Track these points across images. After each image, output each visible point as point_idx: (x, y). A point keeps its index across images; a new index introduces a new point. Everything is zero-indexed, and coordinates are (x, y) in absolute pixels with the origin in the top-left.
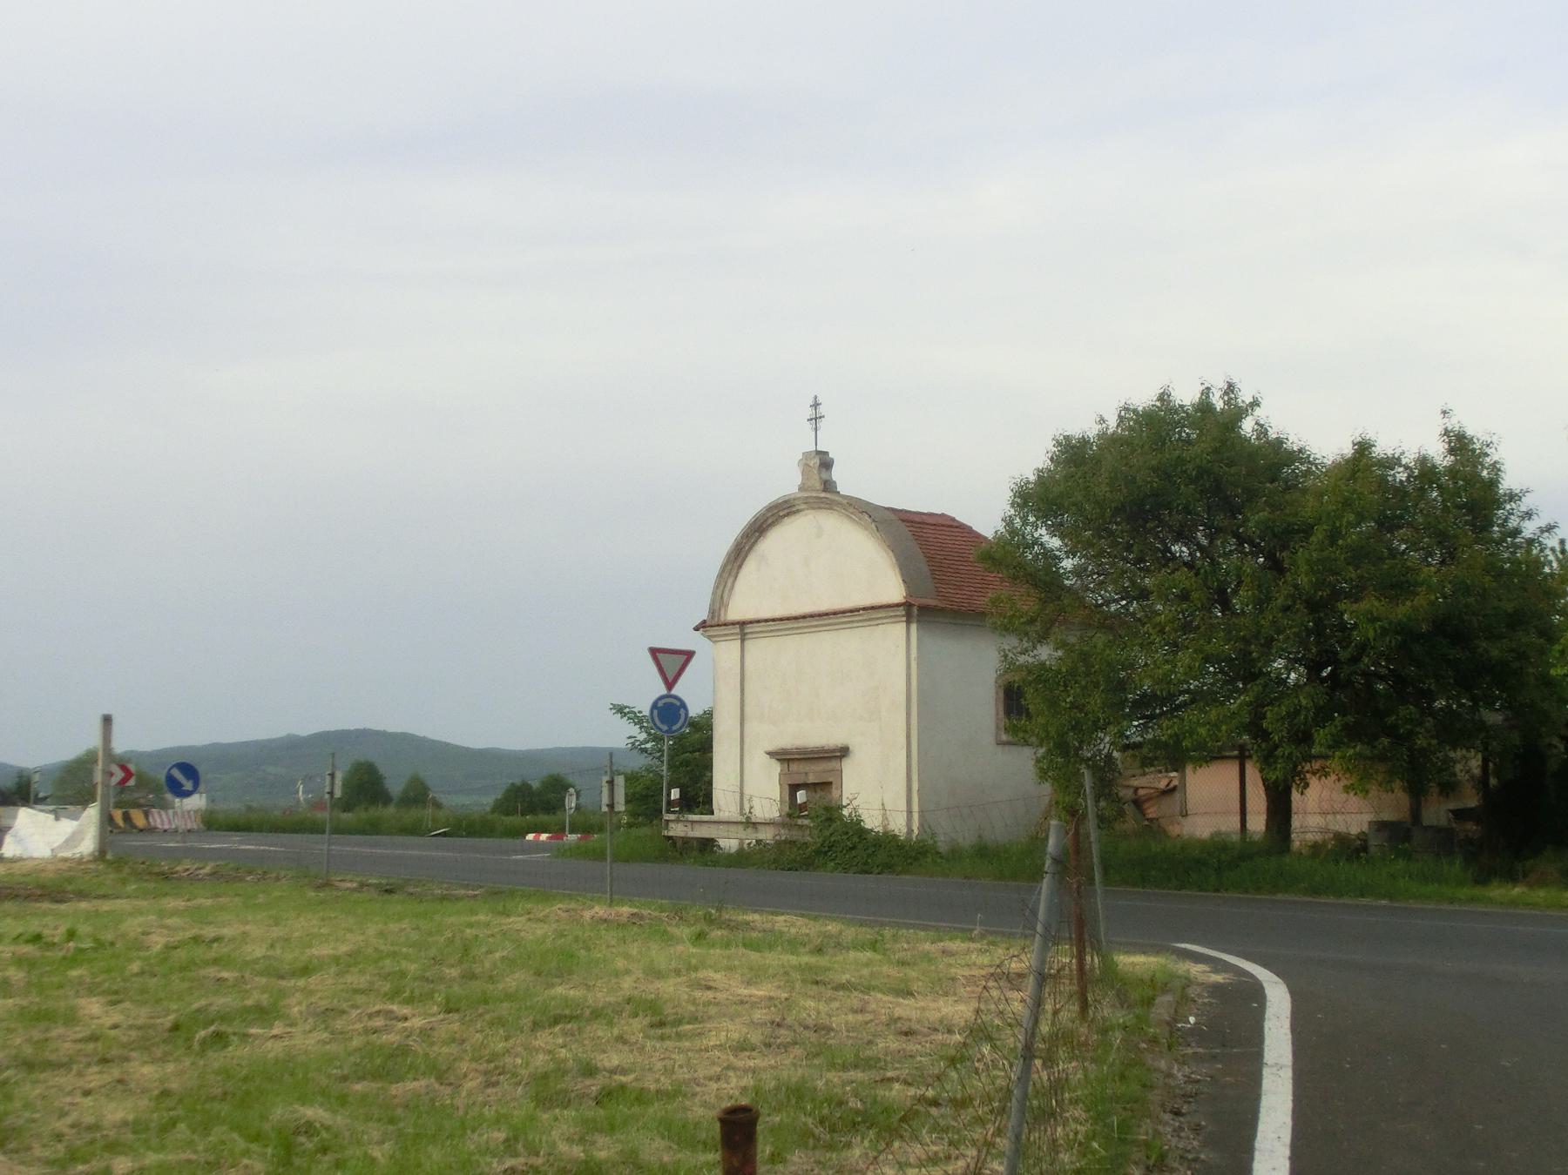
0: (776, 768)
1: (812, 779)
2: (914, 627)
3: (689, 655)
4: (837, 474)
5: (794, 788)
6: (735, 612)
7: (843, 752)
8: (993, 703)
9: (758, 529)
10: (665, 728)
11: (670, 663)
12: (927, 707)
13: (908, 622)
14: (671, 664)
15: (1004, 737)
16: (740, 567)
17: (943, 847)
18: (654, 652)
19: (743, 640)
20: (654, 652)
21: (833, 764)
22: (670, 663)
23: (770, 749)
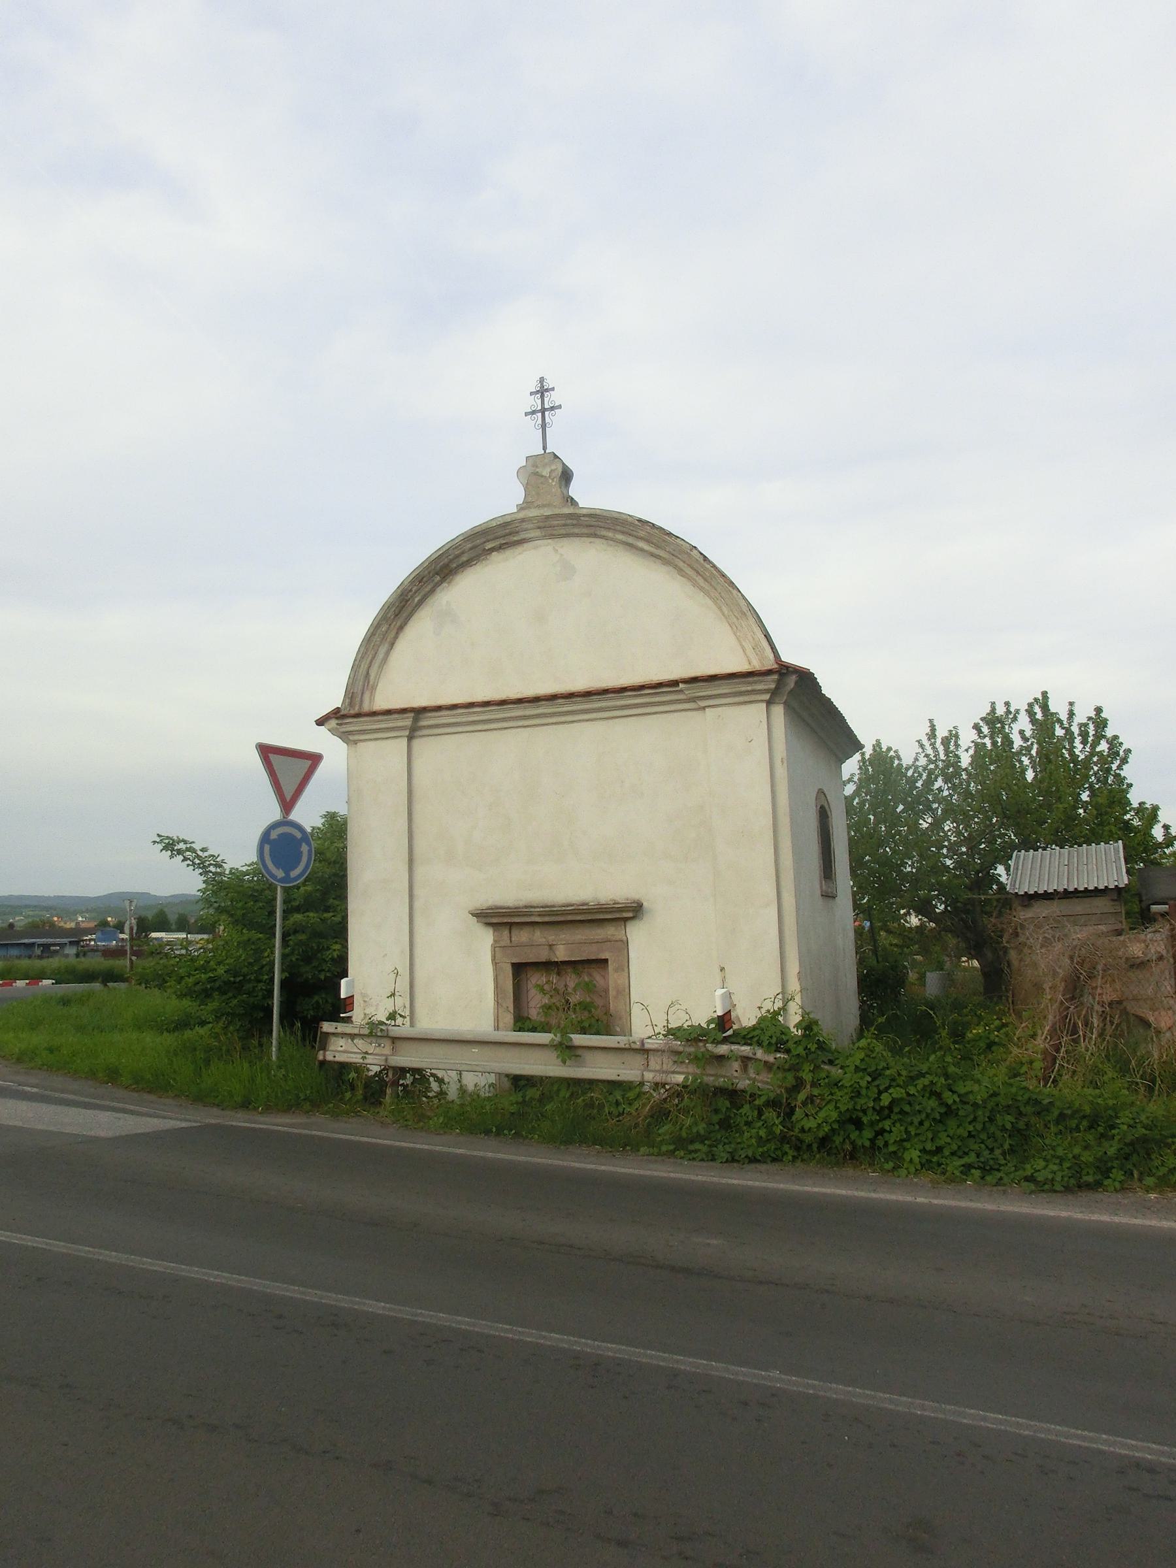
0: (486, 939)
1: (561, 954)
4: (574, 491)
5: (520, 969)
6: (383, 699)
7: (632, 912)
9: (442, 569)
10: (280, 874)
11: (287, 767)
14: (290, 772)
16: (401, 628)
18: (266, 751)
19: (410, 738)
20: (266, 751)
21: (610, 931)
22: (287, 767)
23: (515, 888)
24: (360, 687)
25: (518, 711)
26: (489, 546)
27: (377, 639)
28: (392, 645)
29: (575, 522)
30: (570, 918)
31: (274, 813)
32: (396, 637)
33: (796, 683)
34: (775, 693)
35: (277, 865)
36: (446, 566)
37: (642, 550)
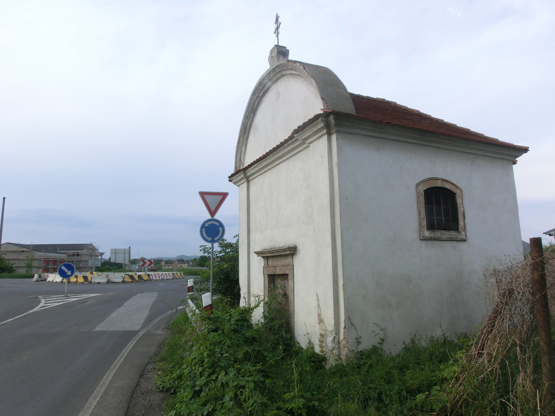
2: (334, 137)
3: (224, 195)
11: (213, 200)
12: (349, 209)
13: (329, 134)
15: (427, 234)
17: (536, 275)
18: (203, 194)
20: (203, 194)
21: (288, 261)
22: (213, 200)
25: (264, 163)
26: (261, 95)
27: (241, 144)
28: (246, 145)
30: (282, 253)
32: (247, 142)
33: (334, 119)
34: (327, 126)
35: (208, 236)
37: (295, 75)
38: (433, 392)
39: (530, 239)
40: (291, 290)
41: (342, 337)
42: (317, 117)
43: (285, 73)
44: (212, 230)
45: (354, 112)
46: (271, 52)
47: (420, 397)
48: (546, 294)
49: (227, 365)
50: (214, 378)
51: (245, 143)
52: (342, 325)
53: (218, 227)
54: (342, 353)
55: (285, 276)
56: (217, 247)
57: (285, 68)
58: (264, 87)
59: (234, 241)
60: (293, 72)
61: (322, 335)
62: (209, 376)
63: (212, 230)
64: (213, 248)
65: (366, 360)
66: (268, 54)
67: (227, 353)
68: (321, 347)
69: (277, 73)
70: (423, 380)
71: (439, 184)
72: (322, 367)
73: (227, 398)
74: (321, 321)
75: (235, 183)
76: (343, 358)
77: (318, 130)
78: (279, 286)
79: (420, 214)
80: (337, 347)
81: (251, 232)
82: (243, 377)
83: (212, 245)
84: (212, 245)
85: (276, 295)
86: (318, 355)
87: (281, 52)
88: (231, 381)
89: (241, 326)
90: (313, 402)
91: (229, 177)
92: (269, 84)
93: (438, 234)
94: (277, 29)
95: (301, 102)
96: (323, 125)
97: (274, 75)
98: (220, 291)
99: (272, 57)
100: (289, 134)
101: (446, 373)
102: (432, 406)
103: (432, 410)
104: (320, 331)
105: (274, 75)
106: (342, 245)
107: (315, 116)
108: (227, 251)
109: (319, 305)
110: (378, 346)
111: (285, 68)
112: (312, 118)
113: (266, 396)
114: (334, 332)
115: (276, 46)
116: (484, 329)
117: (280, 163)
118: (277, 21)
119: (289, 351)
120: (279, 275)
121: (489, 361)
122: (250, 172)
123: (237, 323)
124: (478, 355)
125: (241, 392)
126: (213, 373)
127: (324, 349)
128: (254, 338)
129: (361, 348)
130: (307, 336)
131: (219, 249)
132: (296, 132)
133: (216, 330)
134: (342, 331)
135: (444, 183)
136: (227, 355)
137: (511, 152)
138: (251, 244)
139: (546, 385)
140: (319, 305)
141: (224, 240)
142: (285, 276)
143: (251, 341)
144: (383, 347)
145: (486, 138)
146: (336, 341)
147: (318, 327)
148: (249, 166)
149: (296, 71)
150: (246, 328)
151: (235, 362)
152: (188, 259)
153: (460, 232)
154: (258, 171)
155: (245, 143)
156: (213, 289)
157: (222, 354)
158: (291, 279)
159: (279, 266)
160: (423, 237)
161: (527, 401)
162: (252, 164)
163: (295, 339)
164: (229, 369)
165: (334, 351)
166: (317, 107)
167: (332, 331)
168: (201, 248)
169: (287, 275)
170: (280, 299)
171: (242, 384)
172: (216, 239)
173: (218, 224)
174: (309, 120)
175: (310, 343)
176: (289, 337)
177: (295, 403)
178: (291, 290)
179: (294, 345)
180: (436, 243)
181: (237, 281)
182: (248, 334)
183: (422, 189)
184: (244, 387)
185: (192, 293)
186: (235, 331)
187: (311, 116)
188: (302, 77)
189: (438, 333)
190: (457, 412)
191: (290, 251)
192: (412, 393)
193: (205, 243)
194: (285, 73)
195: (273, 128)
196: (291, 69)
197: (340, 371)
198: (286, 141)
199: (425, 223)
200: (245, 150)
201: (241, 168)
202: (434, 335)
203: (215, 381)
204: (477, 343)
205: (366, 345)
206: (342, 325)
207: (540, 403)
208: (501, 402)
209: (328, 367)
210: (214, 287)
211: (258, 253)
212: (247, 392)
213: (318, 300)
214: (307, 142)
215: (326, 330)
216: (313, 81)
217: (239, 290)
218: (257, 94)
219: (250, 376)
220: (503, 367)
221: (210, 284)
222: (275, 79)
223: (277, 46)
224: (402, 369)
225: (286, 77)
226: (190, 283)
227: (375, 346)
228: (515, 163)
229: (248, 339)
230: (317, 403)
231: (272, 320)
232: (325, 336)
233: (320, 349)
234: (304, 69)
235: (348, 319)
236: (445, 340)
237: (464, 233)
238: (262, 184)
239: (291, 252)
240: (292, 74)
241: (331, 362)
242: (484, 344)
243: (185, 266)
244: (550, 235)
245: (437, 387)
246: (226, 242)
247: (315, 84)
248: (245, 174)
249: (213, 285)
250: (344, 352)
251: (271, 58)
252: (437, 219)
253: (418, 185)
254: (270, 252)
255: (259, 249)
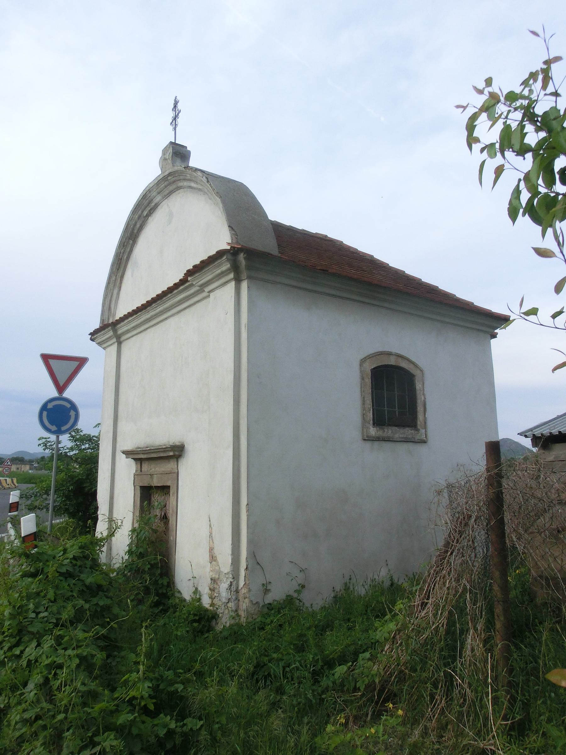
2: (244, 285)
3: (82, 362)
8: (357, 390)
11: (62, 368)
12: (260, 394)
13: (238, 280)
15: (373, 431)
16: (122, 277)
18: (46, 358)
20: (46, 358)
21: (170, 466)
22: (62, 368)
24: (107, 317)
26: (145, 213)
27: (111, 285)
29: (166, 183)
30: (162, 455)
31: (53, 393)
33: (245, 258)
34: (235, 268)
35: (51, 423)
36: (132, 232)
38: (360, 662)
39: (486, 443)
40: (173, 511)
41: (242, 583)
42: (220, 254)
43: (180, 184)
44: (59, 415)
45: (274, 250)
46: (165, 151)
47: (340, 670)
48: (502, 518)
49: (42, 631)
50: (18, 652)
51: (118, 283)
52: (243, 565)
53: (69, 410)
54: (241, 607)
55: (165, 489)
56: (66, 441)
57: (181, 177)
58: (150, 202)
59: (93, 433)
60: (193, 185)
61: (213, 580)
62: (10, 649)
63: (59, 415)
64: (59, 442)
65: (278, 617)
66: (159, 154)
67: (46, 610)
68: (212, 598)
69: (169, 184)
70: (349, 645)
71: (392, 361)
72: (210, 629)
73: (31, 686)
74: (213, 558)
75: (99, 344)
76: (242, 614)
77: (222, 273)
78: (156, 504)
79: (364, 402)
80: (234, 597)
81: (119, 420)
82: (65, 649)
83: (58, 437)
84: (58, 437)
85: (150, 518)
86: (207, 610)
87: (178, 153)
88: (44, 657)
89: (80, 566)
90: (176, 685)
91: (92, 334)
92: (158, 199)
93: (389, 432)
94: (175, 118)
95: (195, 230)
96: (229, 266)
97: (166, 187)
98: (67, 510)
99: (165, 159)
100: (181, 276)
101: (379, 635)
102: (356, 682)
103: (356, 689)
104: (211, 573)
105: (166, 187)
106: (248, 444)
107: (218, 252)
108: (83, 447)
109: (211, 534)
110: (295, 595)
111: (181, 177)
112: (214, 255)
113: (95, 678)
114: (231, 576)
115: (171, 143)
116: (431, 567)
117: (166, 319)
118: (175, 106)
119: (164, 604)
120: (157, 487)
121: (435, 615)
122: (122, 329)
123: (74, 562)
124: (422, 606)
125: (55, 674)
126: (17, 645)
127: (216, 601)
128: (100, 587)
129: (269, 599)
130: (192, 581)
131: (70, 444)
132: (190, 273)
133: (34, 575)
134: (242, 573)
135: (400, 360)
136: (46, 614)
137: (490, 322)
138: (119, 439)
139: (499, 646)
140: (211, 534)
141: (78, 431)
142: (165, 489)
143: (94, 590)
144: (302, 597)
145: (458, 300)
146: (234, 588)
147: (208, 568)
148: (122, 319)
149: (196, 183)
150: (87, 570)
151: (56, 625)
152: (31, 458)
153: (418, 430)
154: (135, 328)
155: (118, 283)
156: (54, 507)
157: (37, 614)
158: (173, 494)
159: (157, 474)
160: (367, 437)
161: (477, 670)
162: (130, 315)
163: (174, 586)
164: (45, 638)
165: (230, 605)
166: (223, 240)
167: (228, 573)
168: (41, 442)
169: (168, 487)
170: (157, 524)
171: (60, 660)
172: (63, 428)
173: (68, 406)
174: (210, 257)
175: (196, 591)
176: (165, 584)
177: (138, 689)
178: (173, 511)
179: (173, 595)
180: (384, 444)
181: (93, 495)
182: (89, 580)
183: (369, 367)
184: (60, 666)
185: (16, 513)
186: (68, 575)
187: (213, 252)
188: (205, 193)
189: (383, 574)
190: (389, 689)
191: (174, 451)
192: (330, 664)
193: (46, 434)
194: (180, 184)
195: (159, 264)
196: (190, 180)
197: (236, 634)
198: (176, 286)
199: (370, 415)
200: (118, 294)
201: (111, 321)
202: (377, 578)
203: (19, 657)
204: (421, 589)
205: (277, 594)
206: (243, 565)
207: (492, 671)
208: (445, 672)
209: (219, 628)
210: (57, 504)
211: (128, 453)
212: (63, 674)
213: (210, 526)
214: (207, 290)
215: (219, 572)
216: (219, 200)
217: (97, 508)
218: (140, 212)
219: (78, 647)
220: (451, 623)
221: (51, 499)
222: (167, 192)
223: (173, 145)
224: (323, 627)
225: (182, 190)
226: (14, 497)
227: (289, 596)
228: (494, 336)
229: (89, 587)
230: (180, 687)
231: (141, 556)
232: (218, 582)
233: (209, 601)
234: (208, 182)
235: (253, 555)
236: (392, 585)
237: (424, 431)
238: (142, 347)
239: (176, 452)
240: (190, 187)
241: (225, 620)
242: (430, 590)
243: (26, 468)
244: (526, 436)
245: (367, 655)
246: (82, 434)
247: (221, 205)
248: (115, 331)
249: (54, 501)
250: (244, 605)
251: (163, 160)
252: (395, 408)
253: (363, 361)
254: (144, 452)
255: (129, 447)
